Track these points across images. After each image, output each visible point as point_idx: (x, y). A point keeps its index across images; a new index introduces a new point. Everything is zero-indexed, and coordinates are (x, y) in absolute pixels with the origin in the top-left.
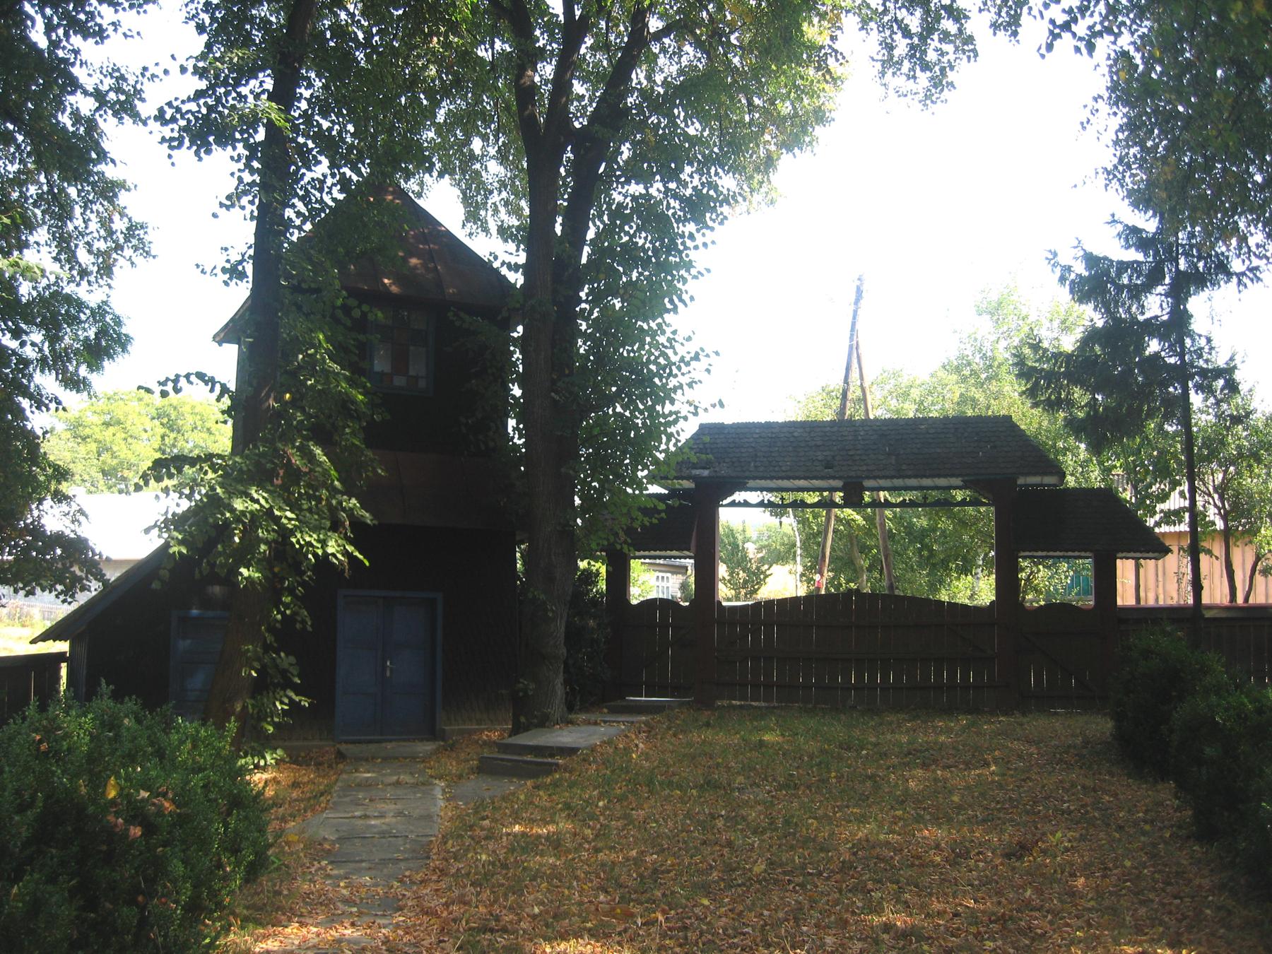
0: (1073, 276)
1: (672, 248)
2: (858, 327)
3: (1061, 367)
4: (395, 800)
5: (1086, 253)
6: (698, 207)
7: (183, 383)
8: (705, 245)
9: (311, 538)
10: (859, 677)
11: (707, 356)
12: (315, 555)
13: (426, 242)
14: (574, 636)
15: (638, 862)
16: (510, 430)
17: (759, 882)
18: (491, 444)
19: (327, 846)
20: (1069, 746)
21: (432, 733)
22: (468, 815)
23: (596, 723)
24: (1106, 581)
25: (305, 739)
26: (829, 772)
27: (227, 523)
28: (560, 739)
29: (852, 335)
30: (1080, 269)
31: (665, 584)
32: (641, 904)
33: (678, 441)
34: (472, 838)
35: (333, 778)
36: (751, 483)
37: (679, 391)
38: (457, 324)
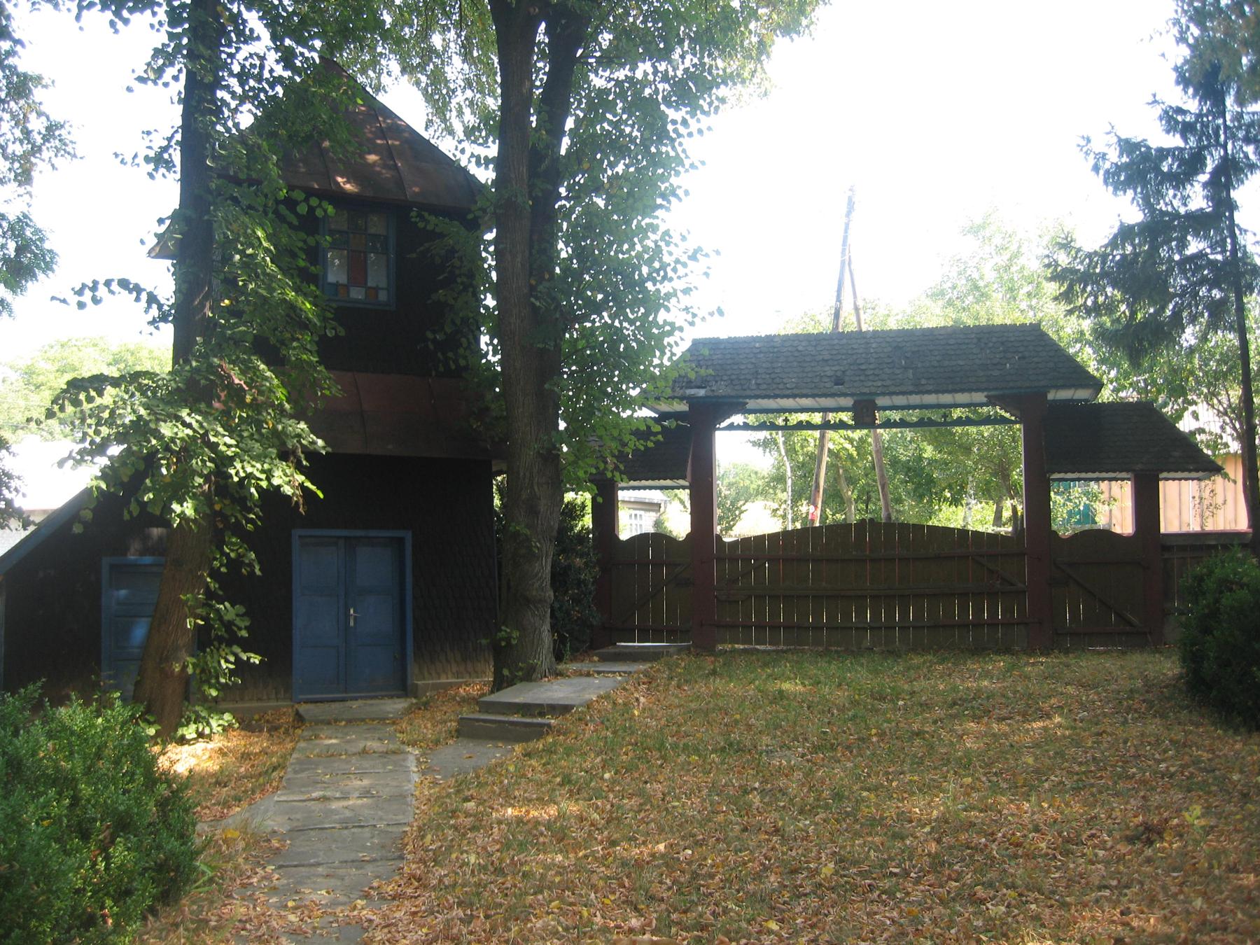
0: (1107, 165)
1: (662, 135)
2: (849, 241)
3: (1095, 267)
4: (361, 775)
5: (1120, 140)
6: (690, 91)
7: (102, 291)
8: (700, 131)
9: (254, 468)
10: (876, 615)
11: (707, 255)
12: (258, 488)
13: (384, 137)
14: (560, 578)
15: (669, 861)
16: (483, 346)
17: (832, 889)
18: (462, 362)
19: (275, 843)
20: (1131, 691)
21: (403, 688)
22: (449, 795)
23: (588, 675)
24: (1147, 506)
25: (260, 700)
26: (868, 729)
27: (153, 453)
28: (549, 694)
29: (844, 250)
30: (1114, 156)
31: (638, 522)
32: (687, 929)
33: (673, 354)
34: (455, 828)
35: (289, 746)
36: (751, 404)
37: (673, 300)
38: (421, 225)
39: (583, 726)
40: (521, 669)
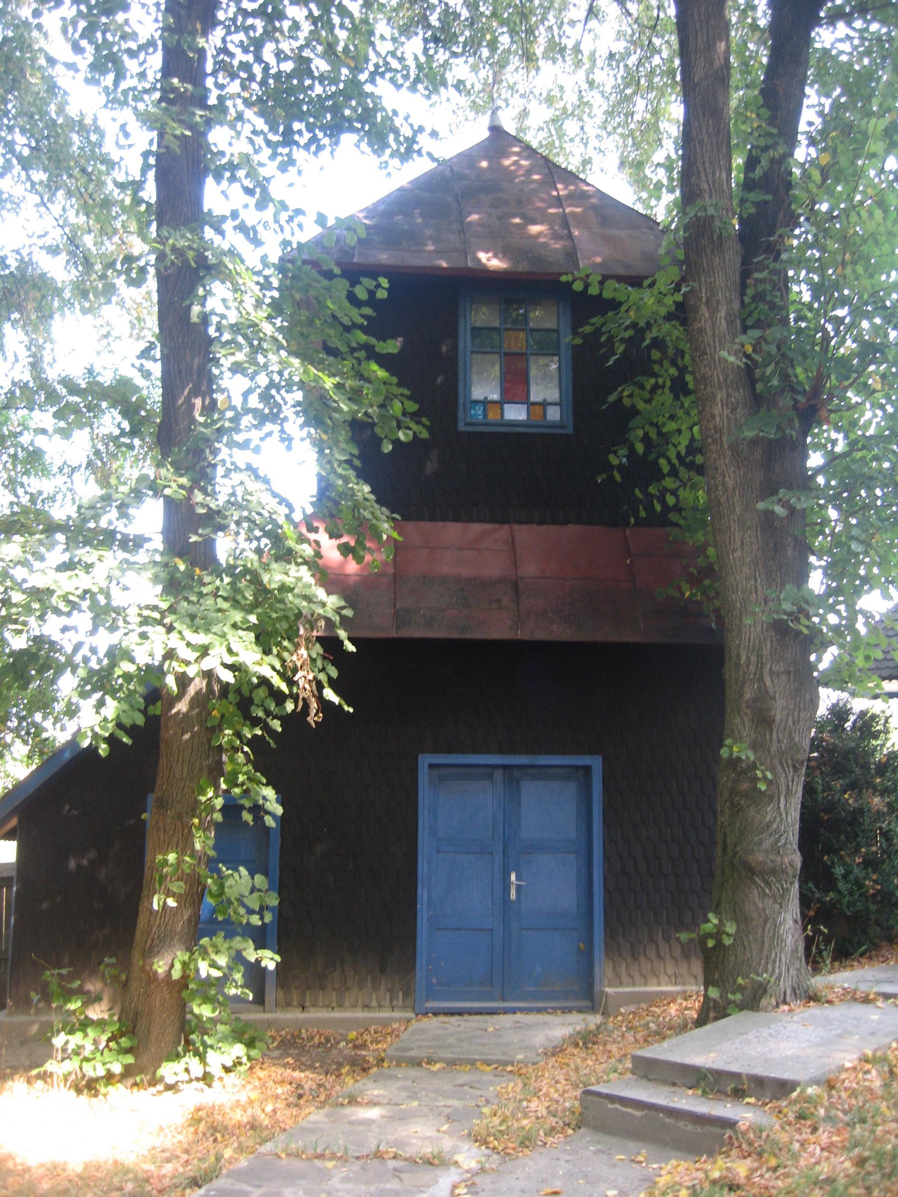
21: (587, 997)
25: (367, 1007)
39: (806, 1135)
40: (741, 989)
